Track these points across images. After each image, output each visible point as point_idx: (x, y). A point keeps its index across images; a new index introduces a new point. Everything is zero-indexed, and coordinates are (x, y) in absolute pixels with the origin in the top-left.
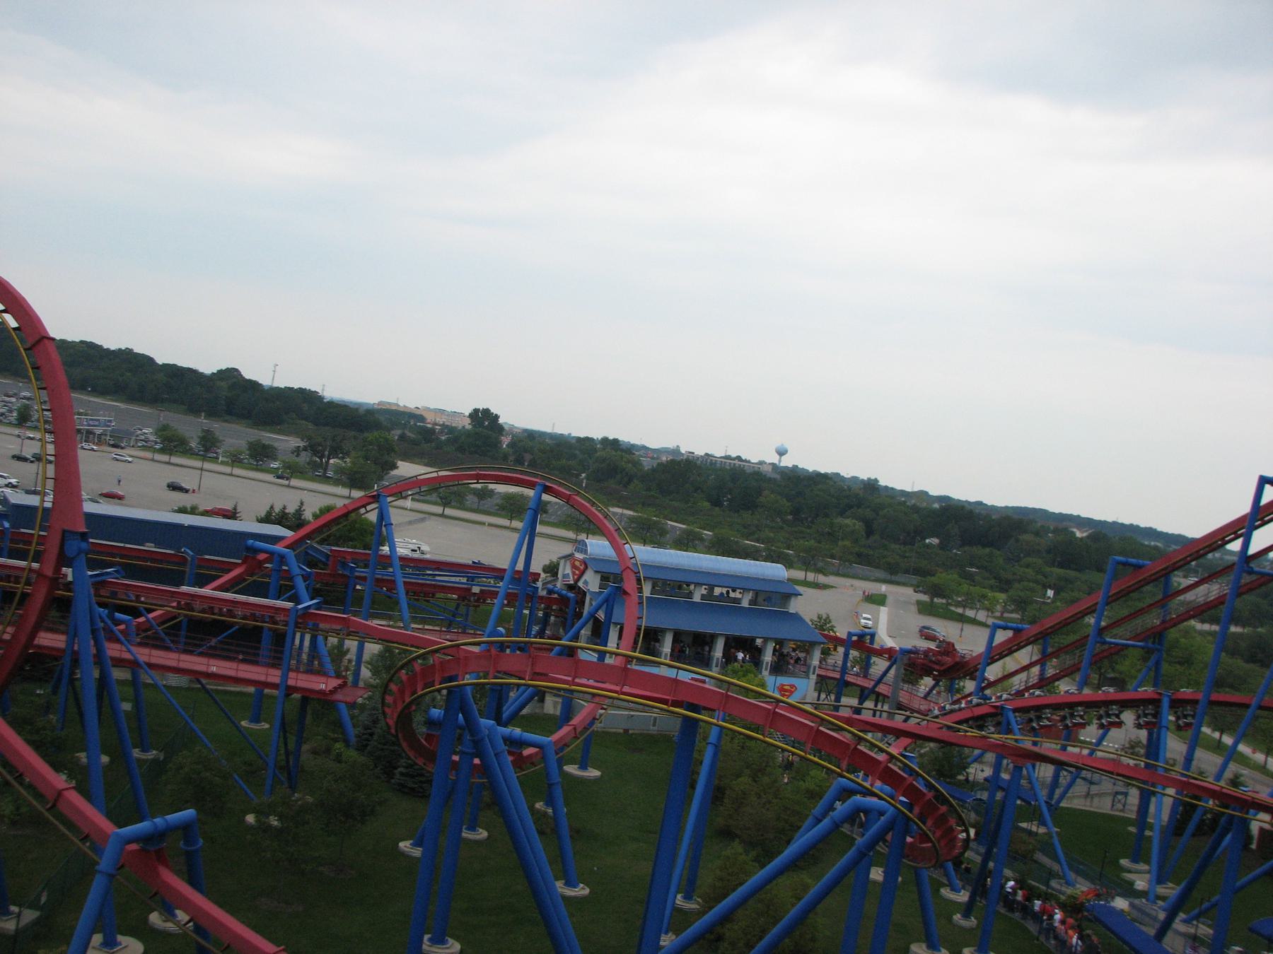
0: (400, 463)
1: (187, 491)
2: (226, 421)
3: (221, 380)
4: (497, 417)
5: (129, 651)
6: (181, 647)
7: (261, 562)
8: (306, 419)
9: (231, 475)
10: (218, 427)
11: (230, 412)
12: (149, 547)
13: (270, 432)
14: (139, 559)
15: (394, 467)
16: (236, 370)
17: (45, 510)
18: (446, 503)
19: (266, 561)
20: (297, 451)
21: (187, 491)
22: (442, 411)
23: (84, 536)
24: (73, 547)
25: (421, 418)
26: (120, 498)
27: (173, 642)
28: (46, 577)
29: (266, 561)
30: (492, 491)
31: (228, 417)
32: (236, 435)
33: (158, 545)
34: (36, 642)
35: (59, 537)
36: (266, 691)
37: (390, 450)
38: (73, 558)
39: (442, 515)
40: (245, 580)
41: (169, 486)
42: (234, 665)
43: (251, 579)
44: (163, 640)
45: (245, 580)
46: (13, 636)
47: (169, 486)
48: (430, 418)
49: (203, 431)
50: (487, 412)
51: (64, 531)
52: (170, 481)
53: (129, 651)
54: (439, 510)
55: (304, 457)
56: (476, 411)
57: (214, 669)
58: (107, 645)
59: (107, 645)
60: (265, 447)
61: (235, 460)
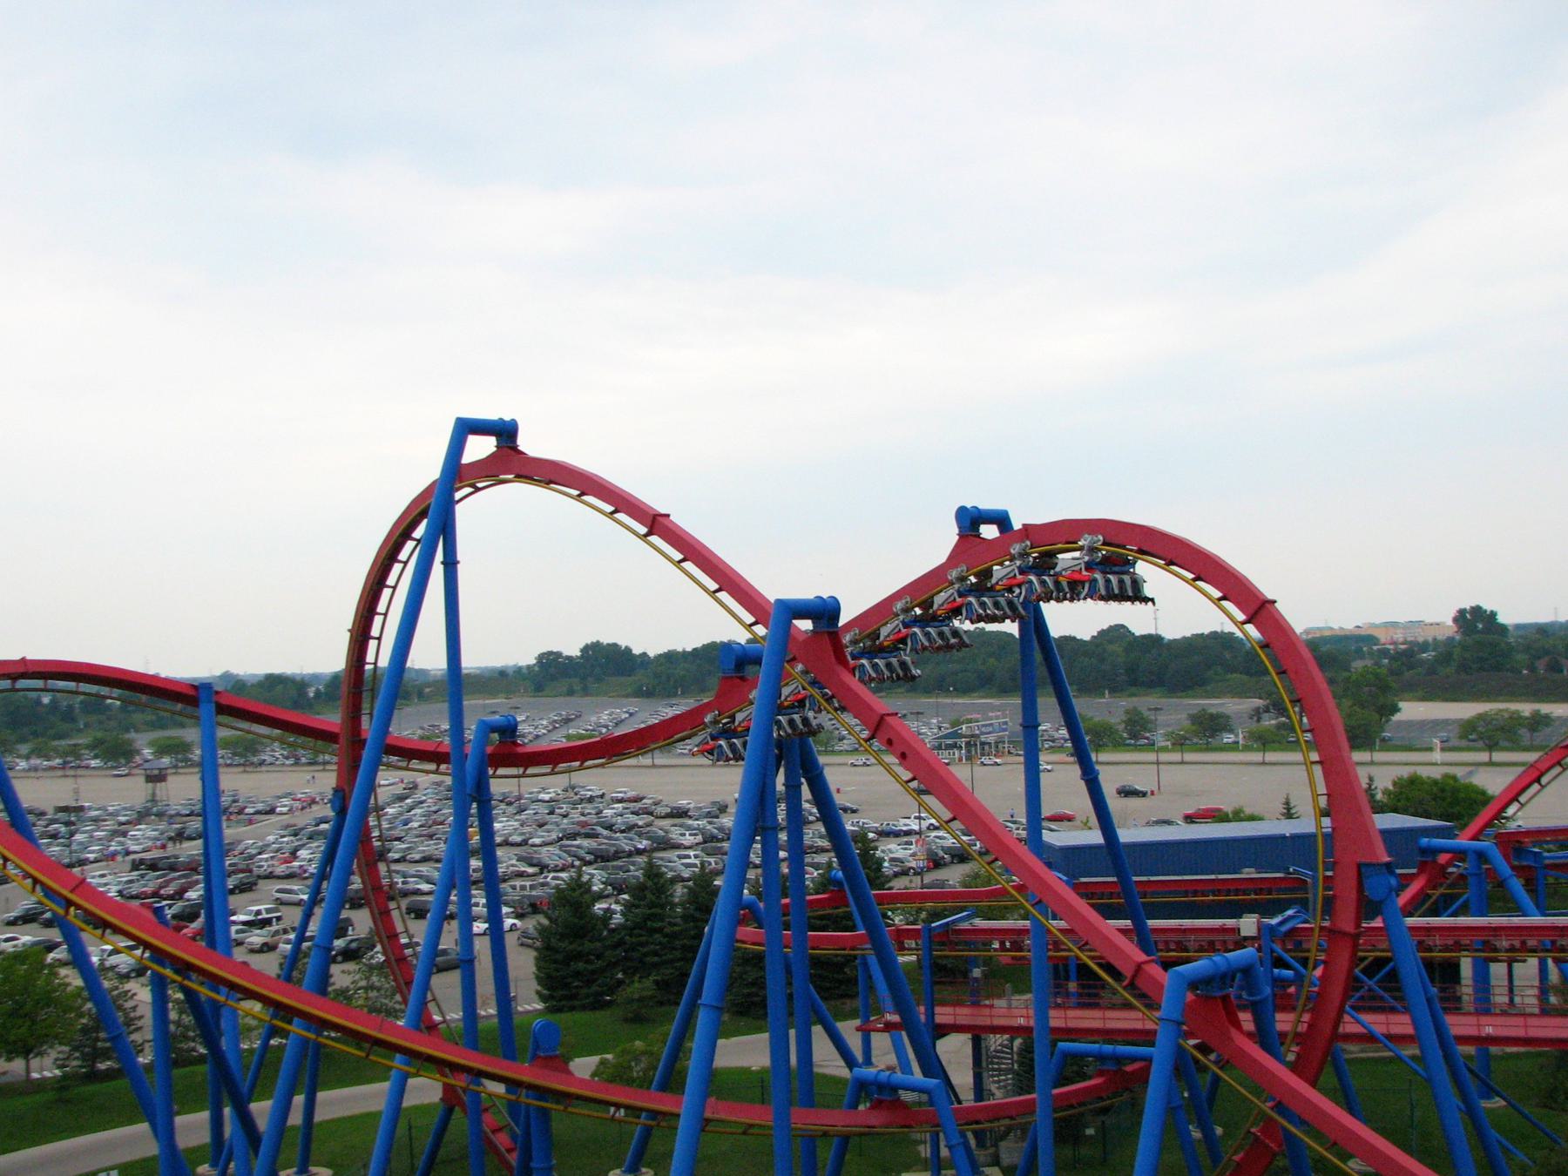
0: (1401, 705)
1: (1144, 794)
2: (1133, 695)
3: (1110, 642)
4: (1493, 615)
5: (1358, 1022)
6: (1073, 1000)
7: (1444, 867)
8: (1233, 670)
9: (1182, 763)
10: (1145, 702)
11: (1134, 683)
12: (1249, 873)
13: (1194, 697)
14: (1176, 893)
15: (1396, 710)
16: (1123, 626)
17: (1325, 835)
18: (1492, 746)
19: (1450, 863)
20: (1257, 714)
21: (1144, 794)
22: (1394, 625)
23: (1389, 867)
24: (1377, 886)
25: (1371, 639)
26: (1070, 819)
27: (1395, 998)
28: (1345, 934)
29: (1450, 863)
30: (1547, 717)
31: (1133, 689)
32: (1173, 712)
33: (1259, 869)
34: (1341, 1030)
35: (1353, 873)
36: (1493, 1050)
37: (1385, 688)
38: (1381, 902)
39: (1491, 764)
40: (1429, 896)
41: (1119, 792)
42: (1097, 1013)
43: (1437, 893)
44: (1382, 998)
45: (1429, 896)
46: (1310, 1026)
47: (1119, 792)
48: (1383, 637)
49: (1127, 712)
50: (1477, 611)
51: (1359, 866)
52: (1118, 785)
53: (1358, 1022)
54: (1483, 756)
55: (1269, 722)
56: (1462, 612)
57: (1489, 1030)
58: (1449, 1020)
59: (1449, 1020)
60: (1213, 717)
61: (1180, 743)
